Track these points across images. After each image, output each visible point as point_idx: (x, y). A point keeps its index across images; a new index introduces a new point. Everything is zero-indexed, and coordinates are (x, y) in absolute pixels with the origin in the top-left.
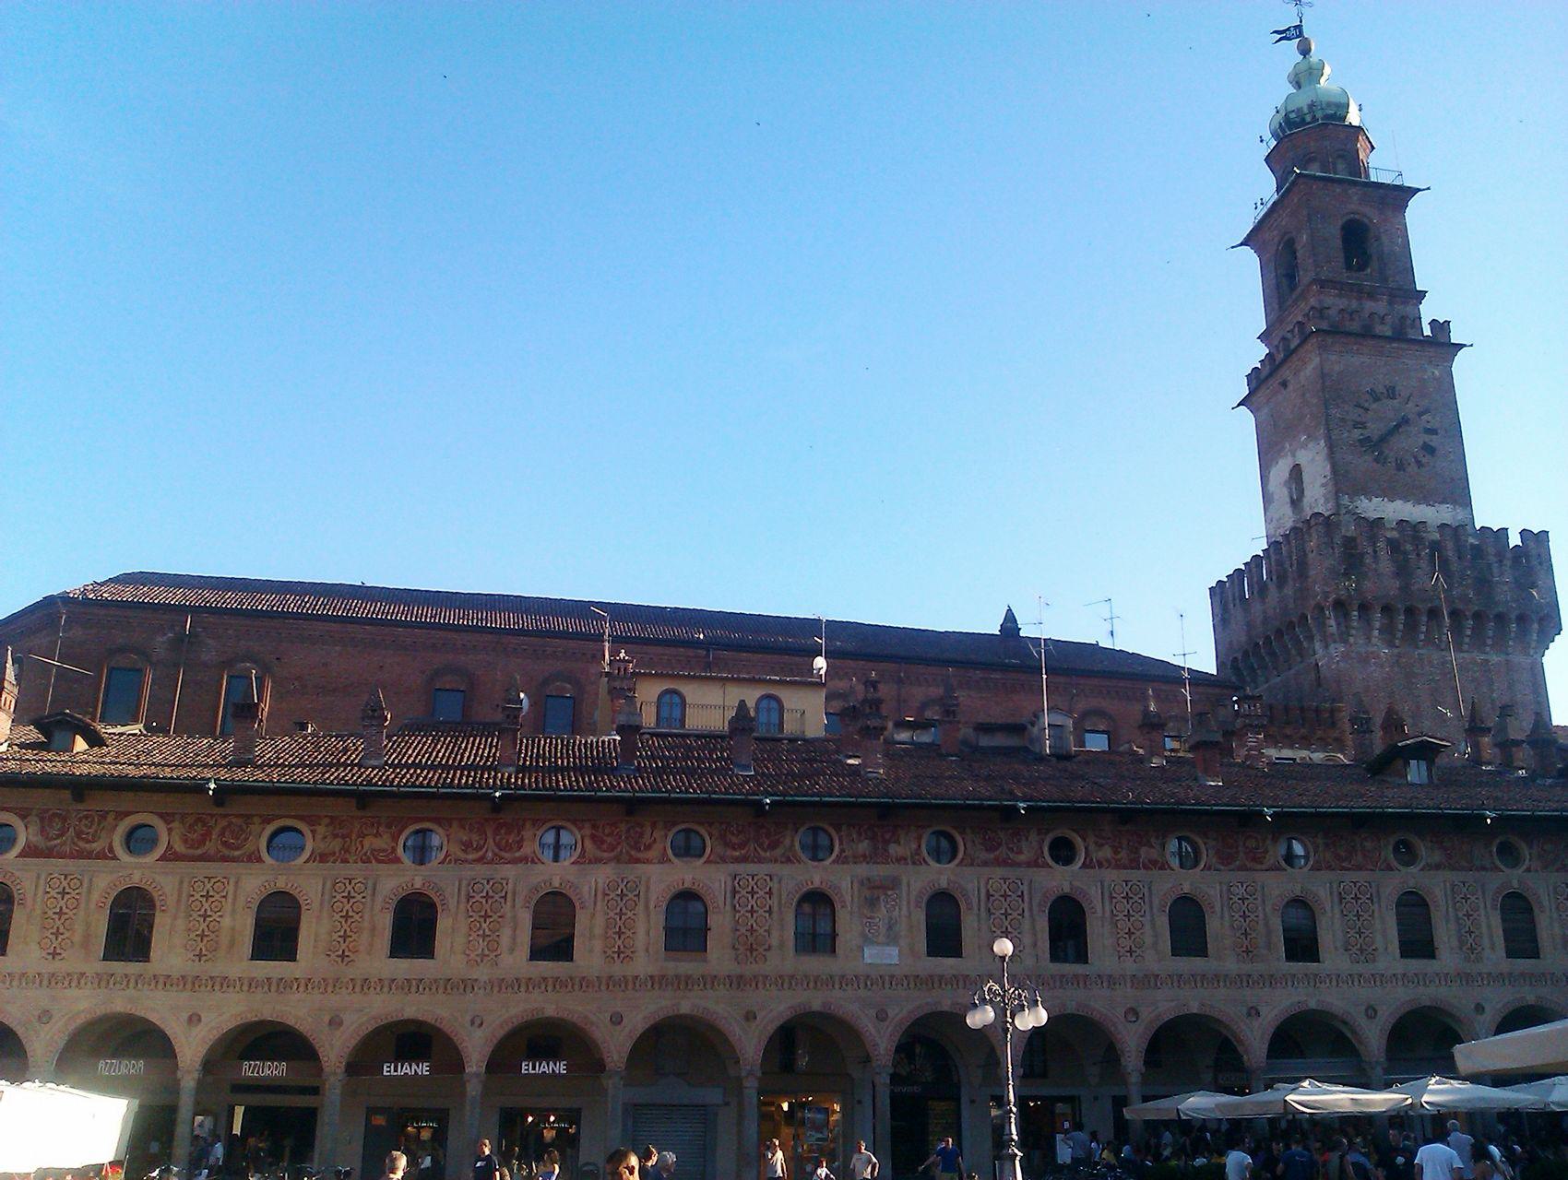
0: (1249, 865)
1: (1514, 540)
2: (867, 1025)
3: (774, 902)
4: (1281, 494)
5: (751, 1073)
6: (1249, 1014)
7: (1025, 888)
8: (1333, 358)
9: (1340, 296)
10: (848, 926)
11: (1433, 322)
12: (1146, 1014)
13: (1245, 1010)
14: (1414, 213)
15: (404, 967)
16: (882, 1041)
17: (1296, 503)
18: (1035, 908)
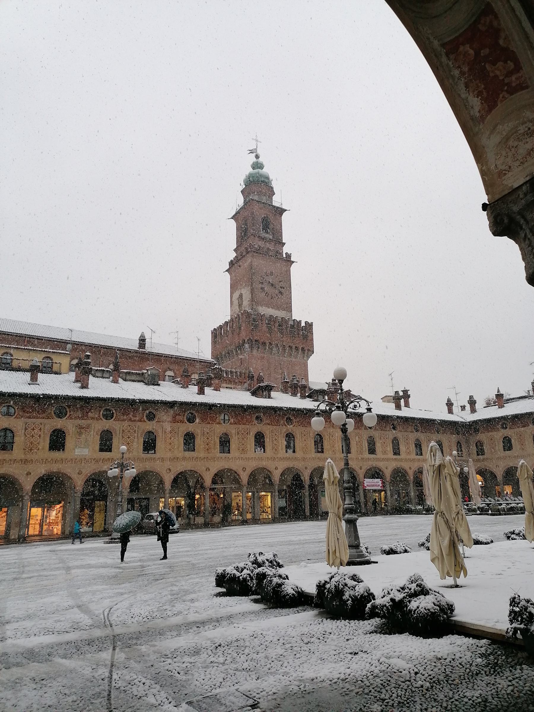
1: (303, 324)
2: (74, 476)
3: (41, 433)
4: (236, 302)
5: (27, 494)
7: (136, 429)
10: (69, 442)
14: (285, 217)
15: (188, 454)
16: (79, 482)
17: (240, 305)
18: (139, 435)
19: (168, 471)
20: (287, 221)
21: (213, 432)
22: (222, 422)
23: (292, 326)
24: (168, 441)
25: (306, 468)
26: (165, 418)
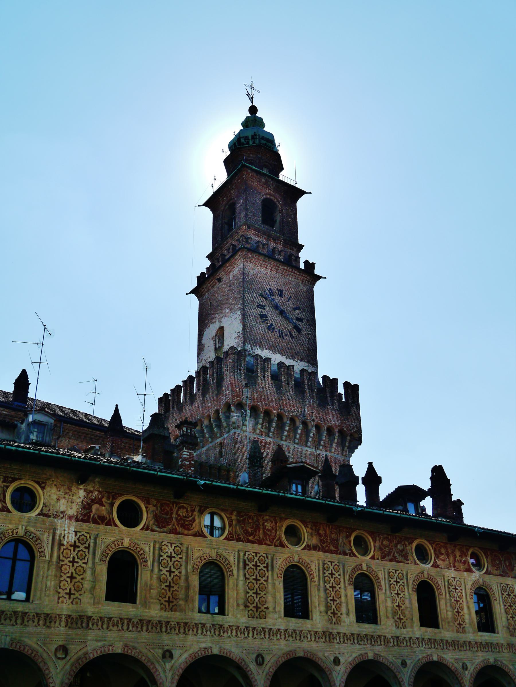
0: (179, 529)
4: (209, 345)
6: (164, 656)
8: (250, 265)
9: (257, 235)
11: (306, 263)
12: (75, 651)
13: (161, 651)
14: (301, 204)
19: (60, 655)
20: (307, 213)
21: (184, 555)
22: (207, 531)
23: (321, 391)
24: (68, 569)
25: (404, 664)
26: (62, 505)
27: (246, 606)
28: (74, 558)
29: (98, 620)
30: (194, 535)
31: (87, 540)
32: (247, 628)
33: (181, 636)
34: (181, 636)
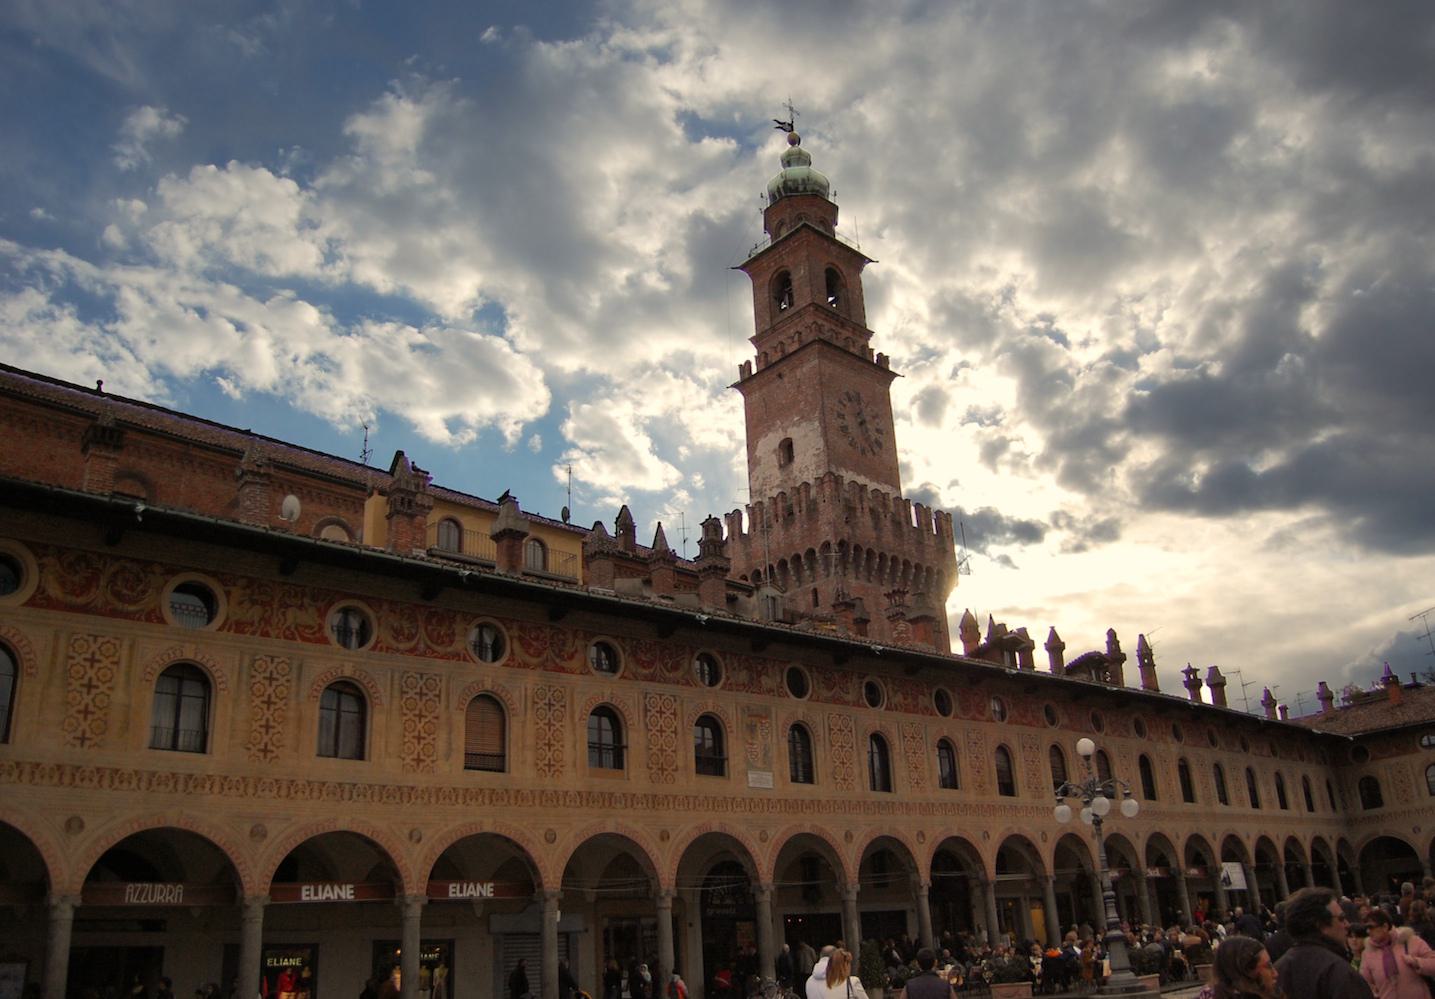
0: (978, 716)
27: (1029, 787)
28: (269, 696)
29: (365, 788)
30: (988, 721)
31: (437, 685)
32: (340, 784)
33: (992, 817)
34: (992, 817)
